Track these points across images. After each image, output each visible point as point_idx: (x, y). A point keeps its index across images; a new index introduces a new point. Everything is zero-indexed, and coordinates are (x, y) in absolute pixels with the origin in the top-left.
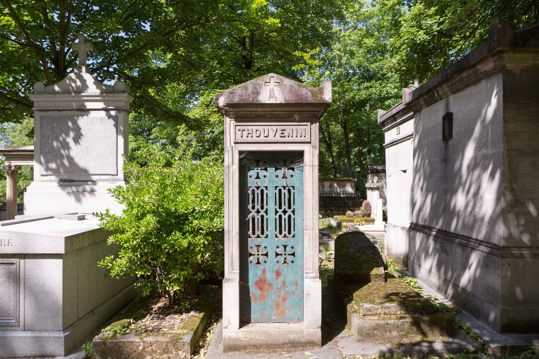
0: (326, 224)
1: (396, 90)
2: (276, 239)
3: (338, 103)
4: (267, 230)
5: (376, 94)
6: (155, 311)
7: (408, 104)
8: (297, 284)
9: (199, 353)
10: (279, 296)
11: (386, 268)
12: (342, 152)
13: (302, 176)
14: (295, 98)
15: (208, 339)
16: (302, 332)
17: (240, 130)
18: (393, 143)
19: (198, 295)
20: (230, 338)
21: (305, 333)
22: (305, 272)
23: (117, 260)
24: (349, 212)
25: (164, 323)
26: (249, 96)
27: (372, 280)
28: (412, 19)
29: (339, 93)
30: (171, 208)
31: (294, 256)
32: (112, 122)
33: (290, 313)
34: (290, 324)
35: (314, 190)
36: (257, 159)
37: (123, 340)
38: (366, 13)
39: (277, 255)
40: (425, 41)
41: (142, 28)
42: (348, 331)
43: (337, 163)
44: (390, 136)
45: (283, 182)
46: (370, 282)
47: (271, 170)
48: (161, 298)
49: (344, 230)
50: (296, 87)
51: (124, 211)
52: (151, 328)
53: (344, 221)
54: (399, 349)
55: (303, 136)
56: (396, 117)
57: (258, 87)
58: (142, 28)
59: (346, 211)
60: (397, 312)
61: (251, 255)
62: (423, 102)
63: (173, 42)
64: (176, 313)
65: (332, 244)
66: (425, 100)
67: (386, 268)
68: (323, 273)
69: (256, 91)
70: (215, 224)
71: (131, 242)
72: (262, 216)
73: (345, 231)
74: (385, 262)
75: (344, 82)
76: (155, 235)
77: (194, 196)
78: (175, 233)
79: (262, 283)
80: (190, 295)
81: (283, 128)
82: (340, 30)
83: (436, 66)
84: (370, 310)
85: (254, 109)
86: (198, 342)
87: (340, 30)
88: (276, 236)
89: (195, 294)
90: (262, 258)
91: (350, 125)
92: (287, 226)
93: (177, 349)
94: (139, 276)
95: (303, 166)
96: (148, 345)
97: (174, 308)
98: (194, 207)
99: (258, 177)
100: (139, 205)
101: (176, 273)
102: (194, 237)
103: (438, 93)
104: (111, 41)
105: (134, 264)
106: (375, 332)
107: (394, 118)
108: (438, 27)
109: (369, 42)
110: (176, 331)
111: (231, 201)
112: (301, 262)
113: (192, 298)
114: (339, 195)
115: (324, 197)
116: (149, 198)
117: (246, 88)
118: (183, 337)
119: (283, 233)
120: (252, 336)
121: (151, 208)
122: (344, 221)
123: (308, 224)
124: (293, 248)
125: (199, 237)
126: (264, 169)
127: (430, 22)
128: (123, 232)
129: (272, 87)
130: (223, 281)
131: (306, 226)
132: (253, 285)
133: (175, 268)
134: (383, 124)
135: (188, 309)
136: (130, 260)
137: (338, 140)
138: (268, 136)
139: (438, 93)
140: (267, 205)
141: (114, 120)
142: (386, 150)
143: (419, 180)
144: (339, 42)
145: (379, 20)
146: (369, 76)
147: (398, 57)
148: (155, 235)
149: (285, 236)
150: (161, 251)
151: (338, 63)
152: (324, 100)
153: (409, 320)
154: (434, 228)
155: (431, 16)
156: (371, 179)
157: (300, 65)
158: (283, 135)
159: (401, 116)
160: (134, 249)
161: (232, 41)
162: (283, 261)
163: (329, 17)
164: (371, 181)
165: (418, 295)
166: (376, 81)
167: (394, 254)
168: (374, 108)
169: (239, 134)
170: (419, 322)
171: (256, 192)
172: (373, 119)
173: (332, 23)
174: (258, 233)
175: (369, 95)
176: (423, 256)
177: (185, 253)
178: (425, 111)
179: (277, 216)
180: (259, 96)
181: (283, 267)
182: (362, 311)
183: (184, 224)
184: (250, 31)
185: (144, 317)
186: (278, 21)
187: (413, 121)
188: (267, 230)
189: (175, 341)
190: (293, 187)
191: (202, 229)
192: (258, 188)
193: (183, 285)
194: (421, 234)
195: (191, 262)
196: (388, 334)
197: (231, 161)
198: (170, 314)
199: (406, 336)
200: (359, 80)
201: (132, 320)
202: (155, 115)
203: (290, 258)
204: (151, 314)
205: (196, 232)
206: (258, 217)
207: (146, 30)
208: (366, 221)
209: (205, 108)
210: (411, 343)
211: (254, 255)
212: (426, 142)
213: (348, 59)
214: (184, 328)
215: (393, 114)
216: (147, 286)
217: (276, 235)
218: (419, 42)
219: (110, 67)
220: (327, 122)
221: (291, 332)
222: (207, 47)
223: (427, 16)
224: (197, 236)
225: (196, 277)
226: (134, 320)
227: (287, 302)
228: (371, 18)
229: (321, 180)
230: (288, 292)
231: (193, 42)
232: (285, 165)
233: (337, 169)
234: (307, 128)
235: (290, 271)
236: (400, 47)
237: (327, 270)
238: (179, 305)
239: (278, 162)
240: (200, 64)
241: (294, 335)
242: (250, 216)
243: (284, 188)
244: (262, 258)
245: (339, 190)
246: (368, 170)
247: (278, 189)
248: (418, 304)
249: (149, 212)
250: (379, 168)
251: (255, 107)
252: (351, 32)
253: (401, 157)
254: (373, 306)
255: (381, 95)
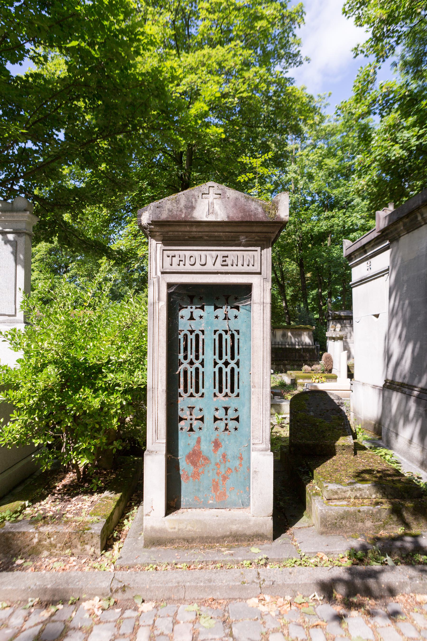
0: (278, 381)
1: (363, 221)
2: (215, 399)
3: (293, 236)
4: (203, 388)
5: (338, 226)
6: (59, 490)
7: (383, 231)
8: (241, 458)
9: (112, 548)
10: (218, 474)
11: (355, 437)
12: (297, 295)
13: (249, 317)
14: (241, 215)
15: (126, 528)
16: (247, 521)
17: (168, 256)
18: (363, 281)
19: (115, 470)
20: (153, 529)
21: (251, 523)
22: (252, 442)
23: (8, 424)
24: (306, 367)
25: (69, 506)
26: (181, 211)
27: (338, 452)
28: (386, 131)
29: (294, 223)
30: (79, 357)
31: (238, 422)
32: (9, 248)
33: (232, 496)
34: (232, 511)
35: (265, 335)
36: (190, 294)
37: (12, 530)
38: (328, 129)
39: (216, 419)
40: (401, 158)
41: (55, 136)
42: (307, 519)
43: (291, 308)
44: (358, 272)
45: (225, 325)
46: (335, 455)
47: (209, 309)
48: (67, 473)
49: (300, 389)
50: (243, 200)
51: (18, 361)
52: (51, 513)
53: (300, 377)
54: (375, 544)
55: (251, 265)
56: (366, 248)
57: (193, 200)
58: (55, 136)
59: (302, 366)
60: (371, 495)
61: (181, 419)
62: (402, 228)
63: (93, 155)
64: (85, 493)
65: (286, 407)
66: (405, 225)
67: (355, 437)
68: (275, 442)
69: (190, 204)
70: (136, 379)
71: (26, 401)
72: (197, 369)
73: (302, 390)
74: (353, 429)
75: (301, 211)
76: (57, 392)
77: (110, 343)
78: (85, 390)
79: (195, 456)
80: (105, 470)
81: (225, 253)
82: (297, 149)
83: (413, 190)
84: (336, 493)
85: (188, 229)
86: (112, 533)
87: (297, 149)
88: (215, 395)
89: (112, 469)
90: (196, 424)
91: (308, 263)
92: (229, 382)
93: (84, 543)
94: (36, 445)
95: (250, 305)
96: (45, 537)
97: (83, 487)
98: (109, 356)
99: (192, 318)
100: (38, 353)
101: (85, 442)
102: (108, 395)
103: (422, 215)
104: (16, 153)
105: (31, 430)
106: (344, 522)
107: (363, 249)
108: (417, 140)
109: (332, 163)
110: (84, 518)
111: (156, 348)
112: (247, 429)
113: (108, 473)
114: (293, 347)
115: (275, 348)
116: (51, 345)
117: (177, 201)
118: (92, 526)
119: (224, 391)
120: (182, 526)
121: (53, 357)
122: (300, 377)
123: (256, 380)
124: (236, 410)
125: (115, 396)
126: (199, 308)
127: (408, 135)
128: (17, 388)
129: (211, 200)
130: (145, 453)
131: (253, 383)
132: (184, 459)
133: (84, 435)
134: (350, 257)
135: (101, 487)
136: (26, 425)
137: (292, 280)
138: (205, 265)
139: (422, 215)
140: (203, 354)
141: (12, 246)
142: (354, 290)
143: (397, 326)
144: (295, 162)
145: (342, 137)
146: (330, 204)
147: (368, 178)
148: (57, 392)
149: (226, 395)
150: (66, 413)
151: (293, 188)
152: (279, 217)
153: (386, 506)
154: (416, 387)
155: (408, 128)
156: (332, 327)
157: (248, 174)
158: (224, 263)
159: (373, 247)
160: (31, 411)
161: (165, 157)
162: (223, 428)
163: (282, 131)
164: (332, 329)
165: (397, 473)
166: (339, 210)
167: (363, 418)
168: (336, 242)
169: (167, 261)
170: (401, 509)
171: (189, 337)
172: (335, 255)
173: (287, 138)
174: (191, 390)
175: (331, 227)
176: (401, 422)
177: (96, 416)
178: (405, 239)
179: (217, 370)
180: (195, 211)
181: (224, 436)
182: (325, 494)
183: (96, 378)
184: (189, 145)
185: (43, 497)
186: (222, 130)
187: (388, 252)
188: (203, 388)
189: (81, 532)
190: (238, 332)
191: (118, 385)
192: (192, 332)
193: (94, 458)
194: (399, 394)
195: (104, 428)
196: (360, 524)
197: (157, 296)
198: (77, 494)
199: (383, 527)
200: (319, 208)
201: (27, 503)
202: (70, 246)
203: (232, 424)
204: (54, 494)
205: (110, 389)
206: (191, 370)
207: (59, 140)
208: (327, 378)
209: (132, 238)
210: (390, 536)
211: (186, 419)
212: (405, 278)
213: (305, 183)
214: (94, 514)
215: (363, 244)
216: (49, 458)
217: (215, 393)
218: (393, 158)
219: (15, 185)
220: (279, 259)
221: (233, 522)
222: (135, 166)
223: (404, 127)
224: (113, 394)
225: (111, 447)
226: (29, 502)
227: (228, 481)
228: (333, 134)
229: (274, 327)
230: (230, 469)
231: (118, 155)
232: (227, 303)
233: (291, 316)
234: (257, 254)
235: (232, 441)
236: (369, 166)
237: (279, 439)
238: (90, 482)
239: (218, 299)
240: (125, 182)
241: (238, 526)
242: (181, 369)
243: (226, 332)
244: (196, 424)
245: (293, 340)
246: (329, 316)
247: (218, 333)
248: (399, 485)
249: (50, 363)
250: (342, 314)
251: (189, 225)
252: (309, 151)
253: (373, 296)
254: (340, 487)
255: (344, 227)
